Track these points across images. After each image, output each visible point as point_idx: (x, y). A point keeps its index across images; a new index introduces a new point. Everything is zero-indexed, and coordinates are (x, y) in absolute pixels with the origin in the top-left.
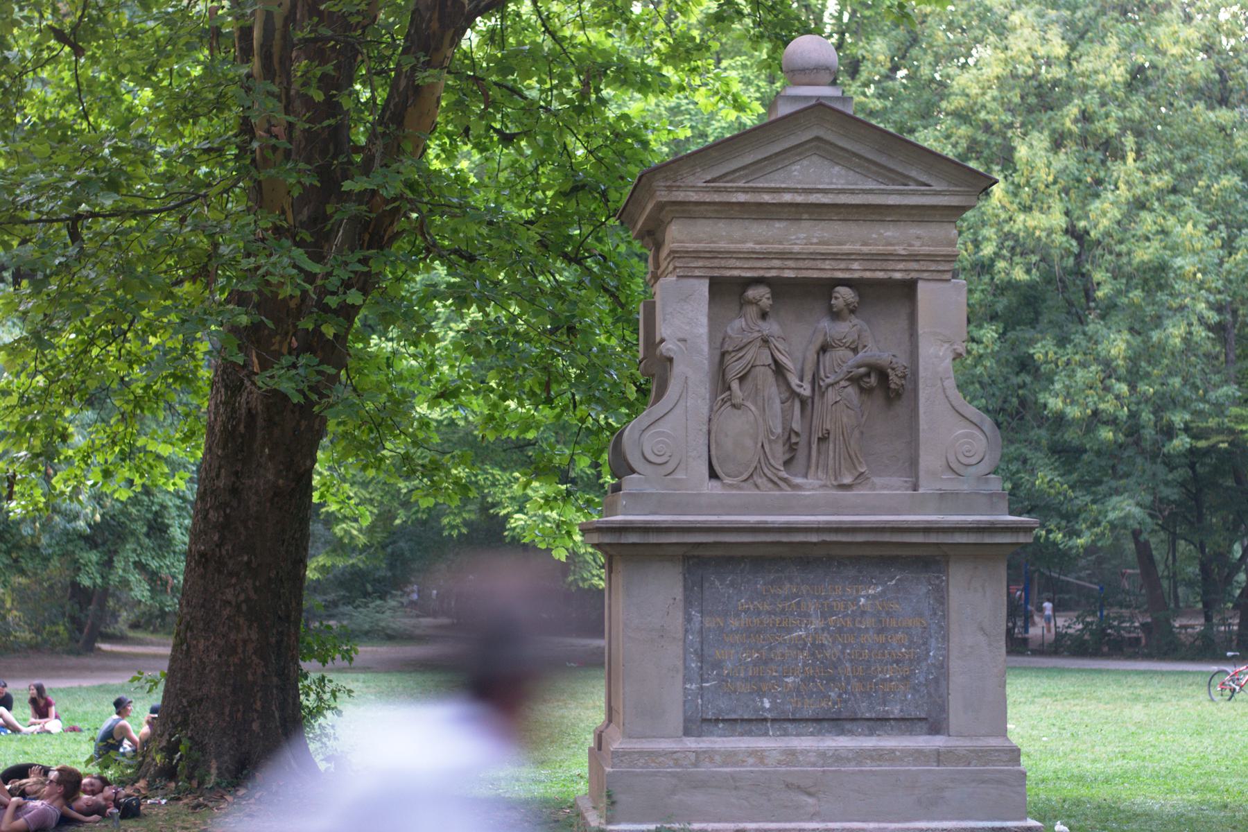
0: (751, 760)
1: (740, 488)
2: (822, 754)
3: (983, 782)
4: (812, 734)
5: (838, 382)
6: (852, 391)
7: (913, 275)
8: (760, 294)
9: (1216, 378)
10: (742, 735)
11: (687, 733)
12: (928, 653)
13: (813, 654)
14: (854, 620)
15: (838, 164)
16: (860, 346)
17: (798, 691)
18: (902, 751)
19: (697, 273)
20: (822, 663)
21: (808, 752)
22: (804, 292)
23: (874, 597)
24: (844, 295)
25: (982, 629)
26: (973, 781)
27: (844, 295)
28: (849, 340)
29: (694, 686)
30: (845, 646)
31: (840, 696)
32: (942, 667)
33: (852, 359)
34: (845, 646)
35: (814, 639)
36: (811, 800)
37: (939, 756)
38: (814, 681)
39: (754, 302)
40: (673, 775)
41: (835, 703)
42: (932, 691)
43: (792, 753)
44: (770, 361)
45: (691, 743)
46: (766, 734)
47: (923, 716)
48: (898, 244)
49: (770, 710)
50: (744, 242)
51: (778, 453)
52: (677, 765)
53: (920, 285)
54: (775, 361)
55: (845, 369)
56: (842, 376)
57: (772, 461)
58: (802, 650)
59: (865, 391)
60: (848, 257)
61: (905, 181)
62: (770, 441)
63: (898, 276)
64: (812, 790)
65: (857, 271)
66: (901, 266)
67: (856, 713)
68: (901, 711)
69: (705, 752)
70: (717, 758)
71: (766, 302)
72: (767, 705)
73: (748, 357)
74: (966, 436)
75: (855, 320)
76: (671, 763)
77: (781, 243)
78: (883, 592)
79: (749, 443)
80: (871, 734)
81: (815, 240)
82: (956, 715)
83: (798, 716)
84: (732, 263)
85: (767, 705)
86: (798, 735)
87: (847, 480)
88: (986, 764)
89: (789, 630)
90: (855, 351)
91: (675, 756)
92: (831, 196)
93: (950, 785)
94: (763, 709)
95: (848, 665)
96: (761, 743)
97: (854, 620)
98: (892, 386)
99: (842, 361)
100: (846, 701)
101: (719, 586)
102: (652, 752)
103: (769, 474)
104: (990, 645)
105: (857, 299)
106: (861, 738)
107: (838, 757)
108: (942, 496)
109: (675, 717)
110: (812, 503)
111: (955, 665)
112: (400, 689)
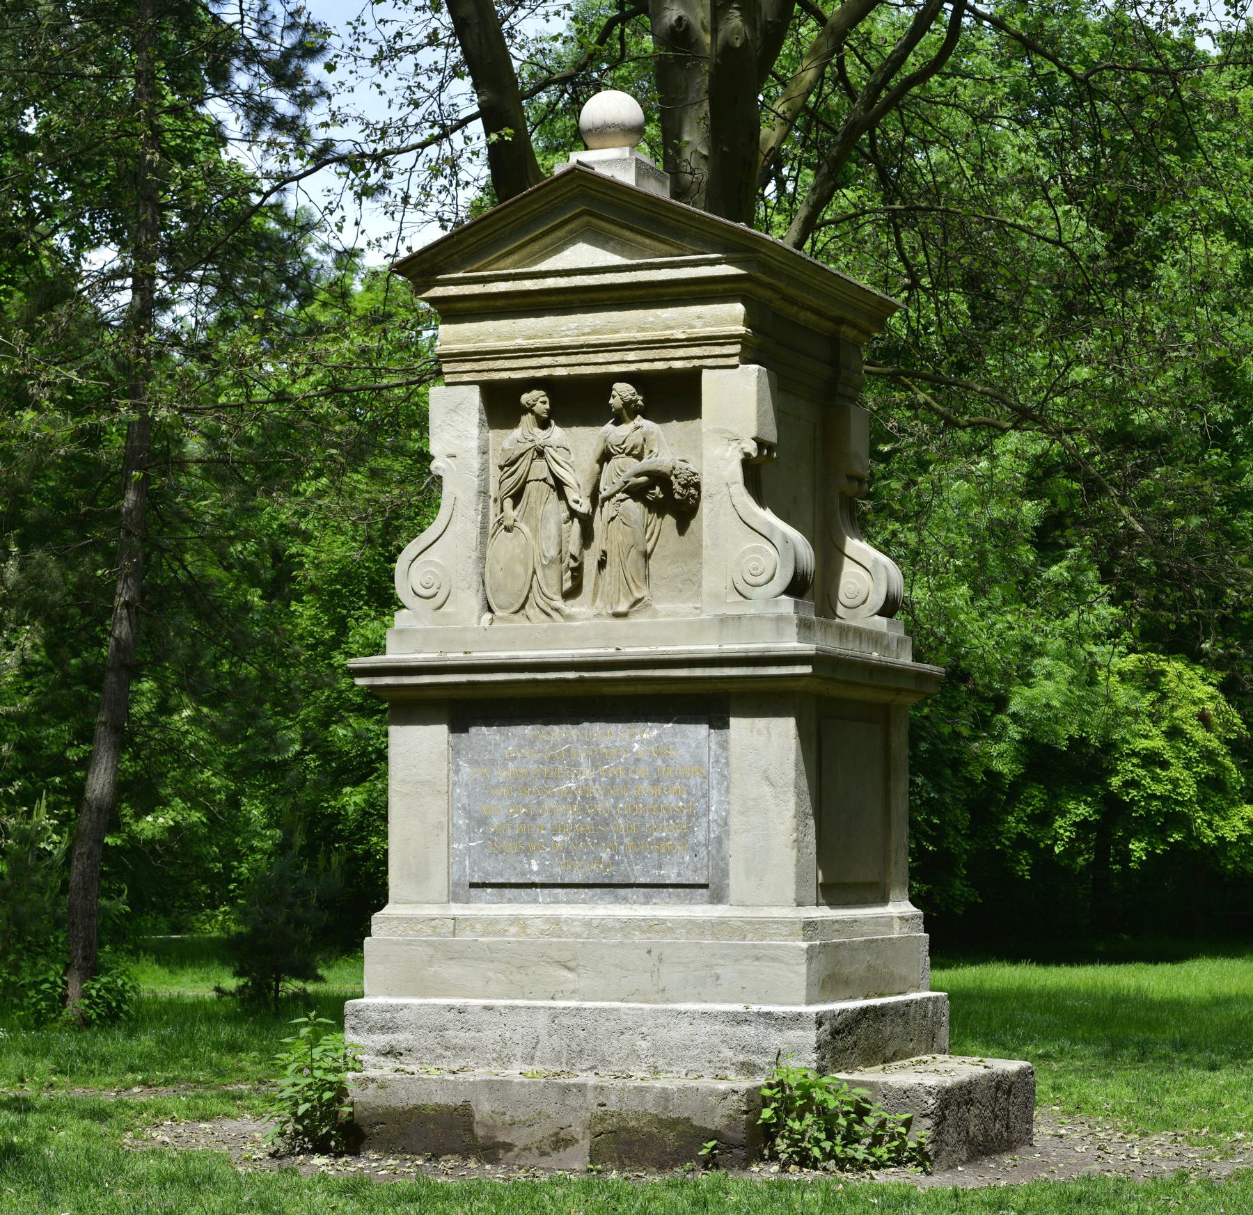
0: (513, 930)
1: (511, 621)
2: (588, 923)
4: (584, 902)
5: (613, 495)
6: (634, 508)
7: (696, 363)
9: (238, 26)
10: (510, 901)
11: (454, 898)
12: (708, 807)
13: (583, 810)
14: (627, 770)
16: (646, 452)
17: (568, 852)
19: (466, 378)
20: (593, 819)
21: (573, 920)
23: (649, 742)
24: (623, 391)
25: (767, 778)
26: (746, 957)
27: (623, 391)
28: (629, 445)
29: (461, 846)
30: (617, 799)
31: (612, 857)
32: (726, 824)
33: (633, 465)
34: (617, 799)
35: (585, 792)
36: (570, 975)
37: (718, 927)
38: (584, 841)
39: (529, 409)
40: (429, 944)
41: (606, 866)
42: (714, 852)
43: (556, 921)
44: (546, 474)
45: (456, 910)
46: (535, 901)
47: (703, 881)
48: (678, 327)
49: (538, 873)
50: (512, 339)
51: (552, 582)
52: (435, 933)
53: (705, 372)
55: (621, 479)
56: (617, 487)
57: (545, 589)
58: (572, 804)
62: (543, 566)
63: (678, 365)
64: (572, 964)
65: (635, 361)
67: (629, 878)
68: (679, 874)
69: (466, 920)
70: (478, 926)
72: (535, 868)
73: (520, 472)
74: (754, 550)
75: (639, 420)
76: (430, 931)
77: (550, 336)
78: (659, 735)
79: (519, 569)
80: (647, 903)
81: (587, 330)
82: (737, 883)
83: (566, 881)
85: (535, 868)
86: (568, 902)
87: (622, 608)
88: (763, 938)
89: (557, 780)
90: (639, 457)
91: (433, 923)
93: (722, 962)
94: (531, 871)
95: (621, 821)
96: (528, 910)
97: (627, 770)
98: (677, 496)
99: (624, 469)
100: (618, 864)
101: (483, 735)
102: (411, 919)
103: (542, 604)
104: (776, 797)
106: (635, 907)
107: (603, 927)
108: (723, 620)
109: (439, 883)
110: (582, 634)
111: (735, 822)
112: (642, 900)
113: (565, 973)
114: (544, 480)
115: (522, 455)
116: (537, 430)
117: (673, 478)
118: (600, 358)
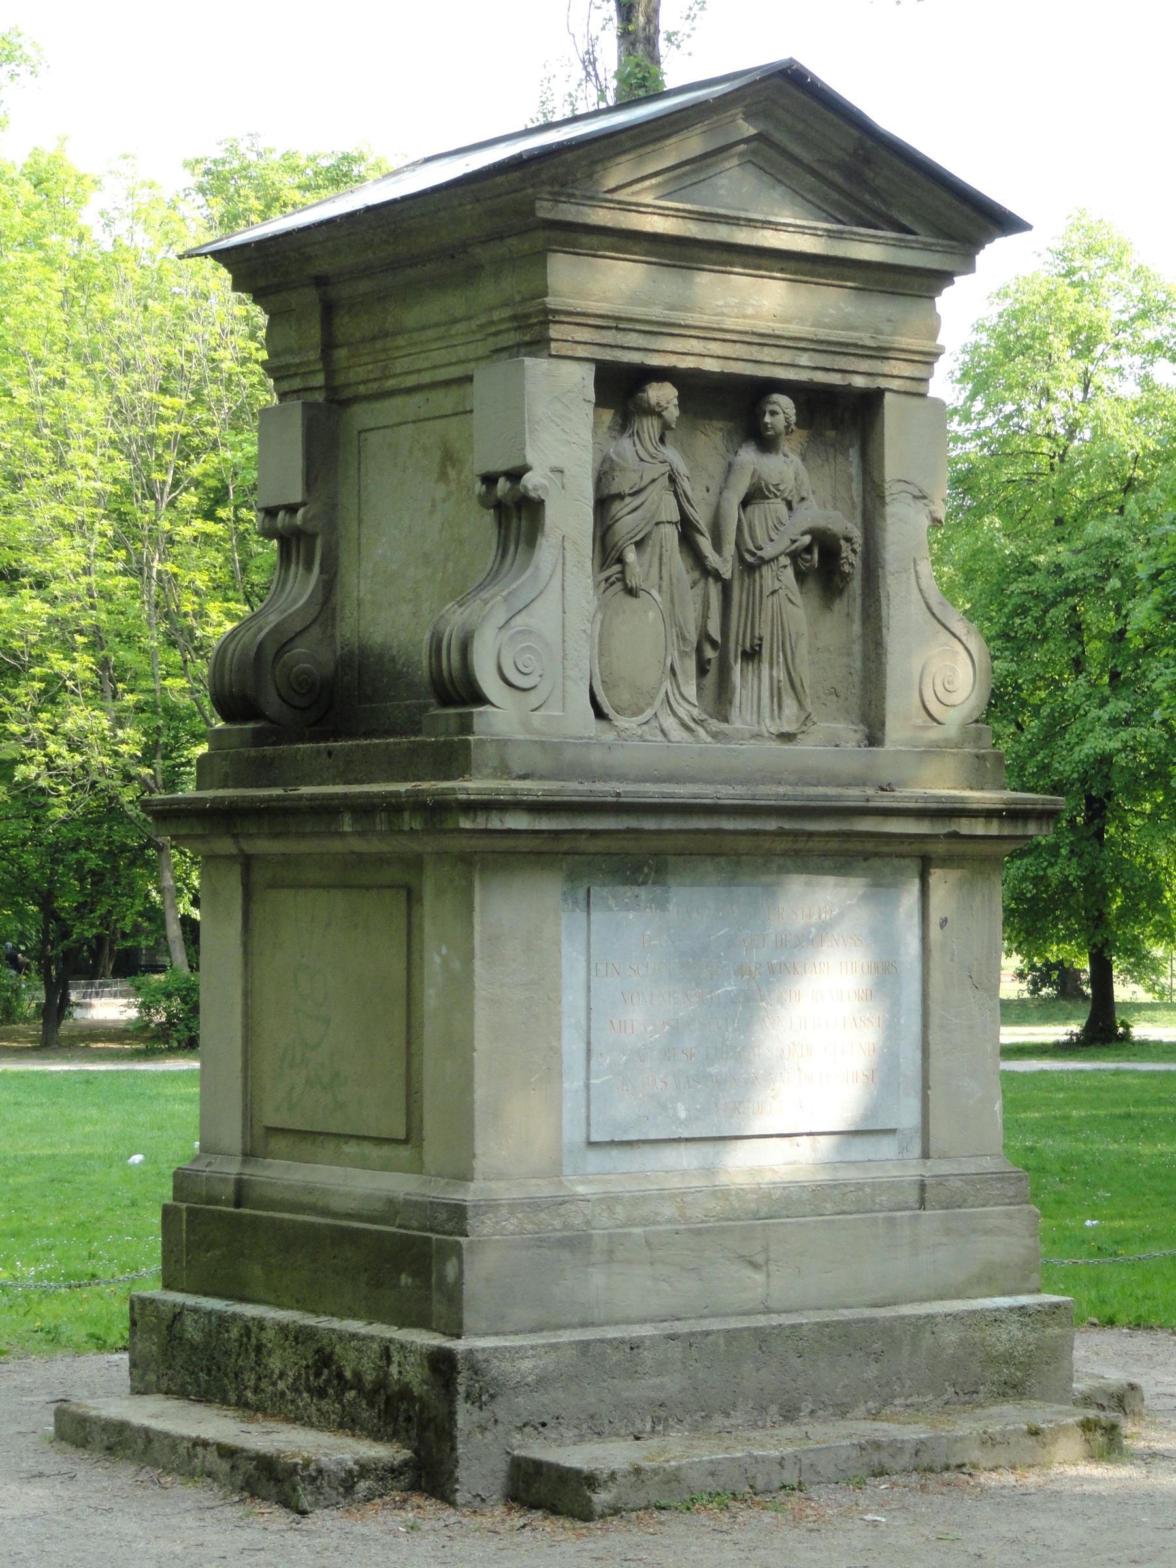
3: (986, 1232)
8: (663, 394)
15: (780, 181)
18: (873, 1186)
19: (581, 352)
22: (732, 403)
26: (974, 1231)
36: (759, 1277)
53: (888, 395)
61: (869, 217)
64: (760, 1259)
65: (801, 369)
71: (672, 413)
84: (633, 339)
92: (783, 235)
113: (749, 1272)
115: (654, 481)
117: (842, 542)
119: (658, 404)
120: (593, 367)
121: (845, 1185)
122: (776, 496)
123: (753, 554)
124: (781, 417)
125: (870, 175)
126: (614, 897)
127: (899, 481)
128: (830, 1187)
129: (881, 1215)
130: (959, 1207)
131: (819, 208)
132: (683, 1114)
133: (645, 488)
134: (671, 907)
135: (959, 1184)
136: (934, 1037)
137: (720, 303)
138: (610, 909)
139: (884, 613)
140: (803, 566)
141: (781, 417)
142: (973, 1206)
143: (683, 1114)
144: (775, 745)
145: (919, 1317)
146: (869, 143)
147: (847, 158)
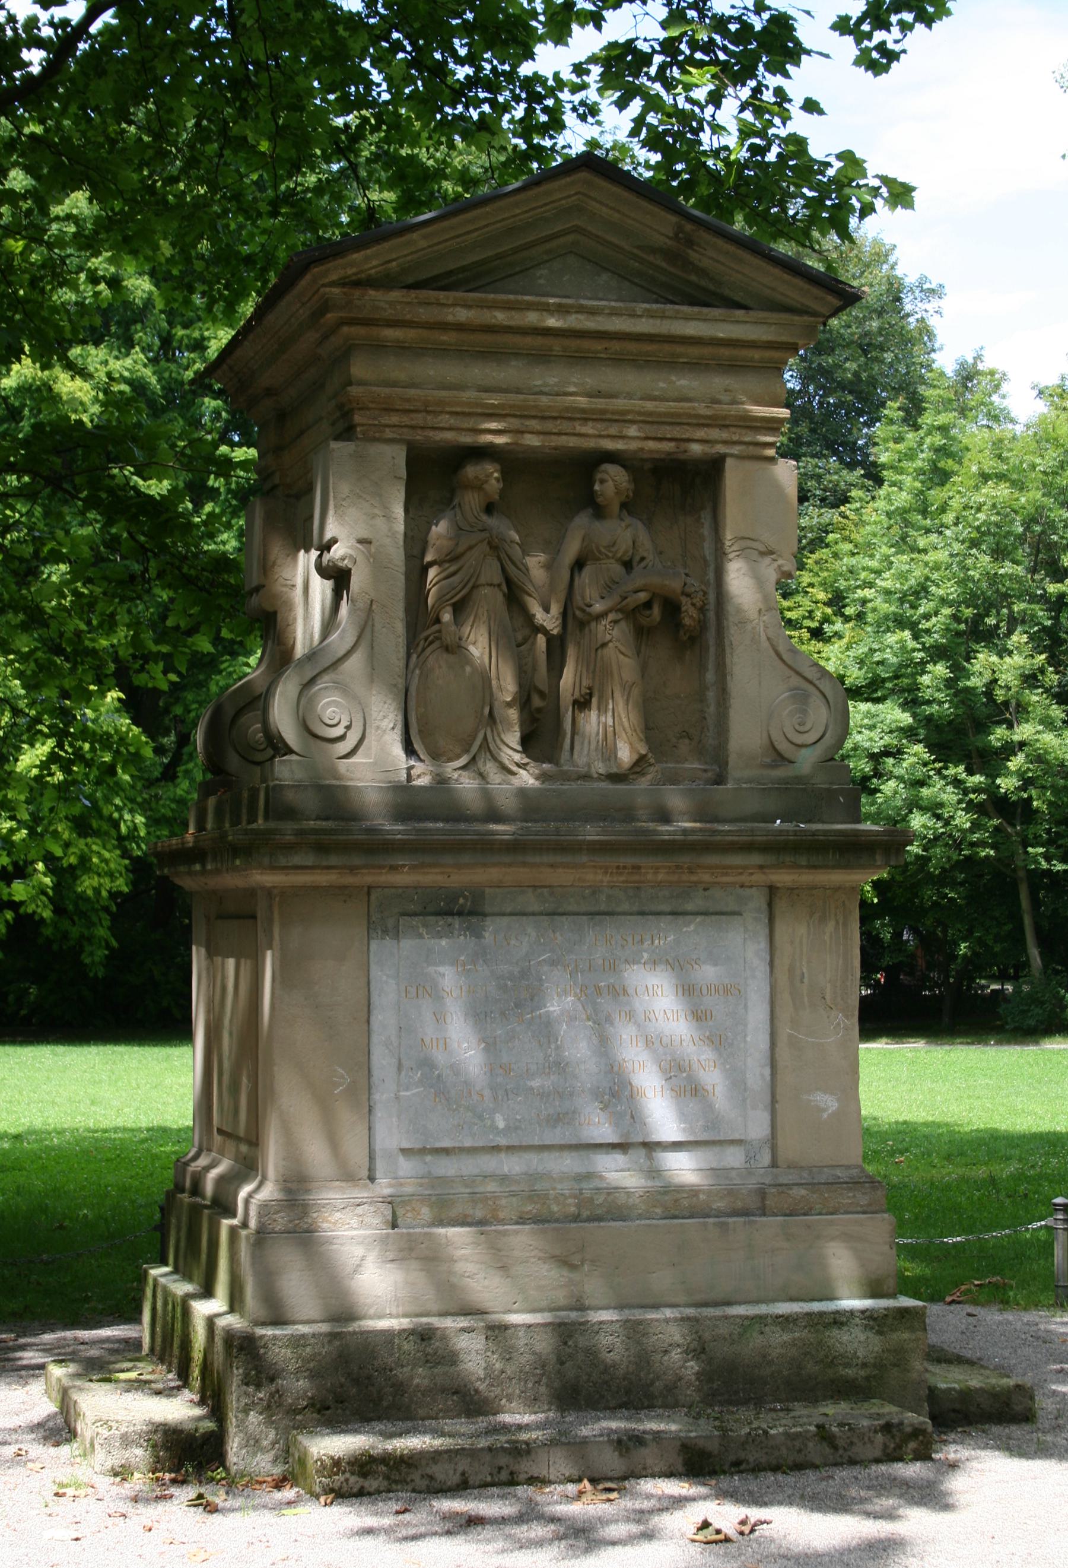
7: (722, 449)
16: (637, 558)
19: (389, 434)
22: (565, 481)
24: (612, 482)
44: (498, 578)
53: (729, 463)
54: (509, 581)
59: (642, 633)
60: (621, 418)
63: (696, 448)
65: (631, 440)
66: (700, 434)
98: (687, 621)
105: (632, 486)
114: (499, 585)
116: (484, 517)
118: (588, 429)
119: (476, 477)
120: (404, 448)
121: (678, 1192)
122: (608, 557)
123: (584, 611)
124: (610, 483)
125: (693, 255)
126: (425, 926)
127: (743, 538)
128: (659, 1193)
129: (711, 1220)
130: (805, 1214)
131: (649, 290)
132: (501, 1124)
133: (462, 554)
134: (487, 935)
135: (803, 1192)
136: (784, 1054)
137: (539, 383)
138: (421, 936)
139: (728, 661)
140: (644, 621)
141: (610, 483)
142: (820, 1214)
143: (501, 1124)
144: (603, 785)
145: (747, 1317)
146: (689, 227)
147: (669, 242)
